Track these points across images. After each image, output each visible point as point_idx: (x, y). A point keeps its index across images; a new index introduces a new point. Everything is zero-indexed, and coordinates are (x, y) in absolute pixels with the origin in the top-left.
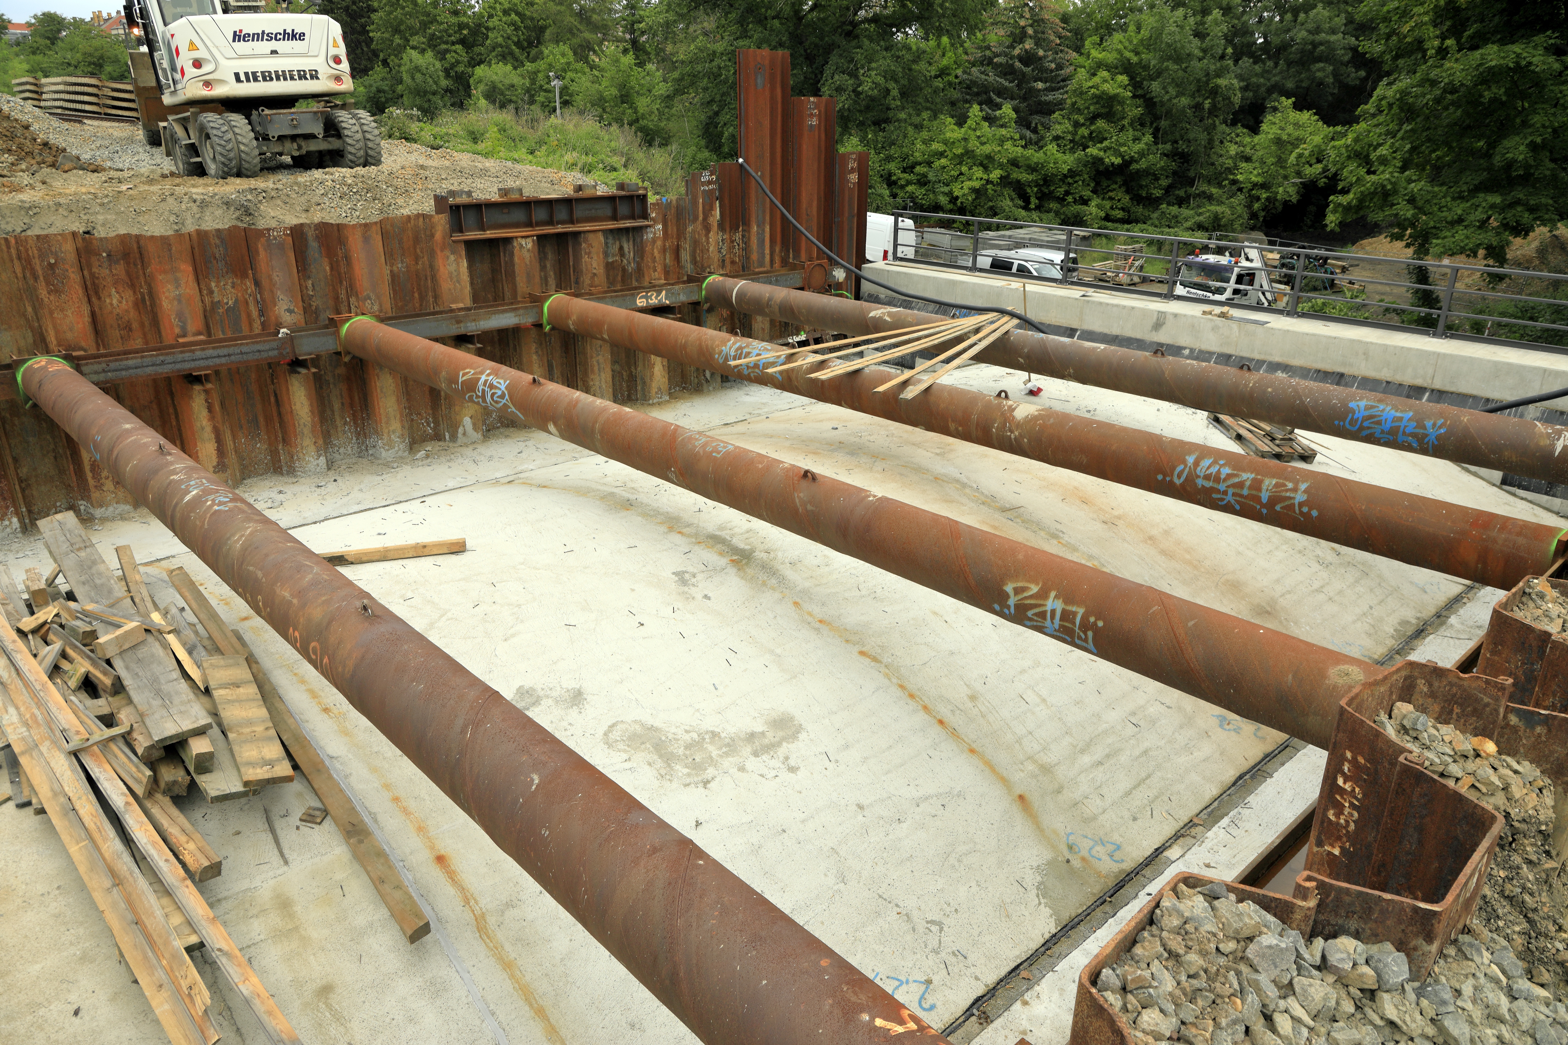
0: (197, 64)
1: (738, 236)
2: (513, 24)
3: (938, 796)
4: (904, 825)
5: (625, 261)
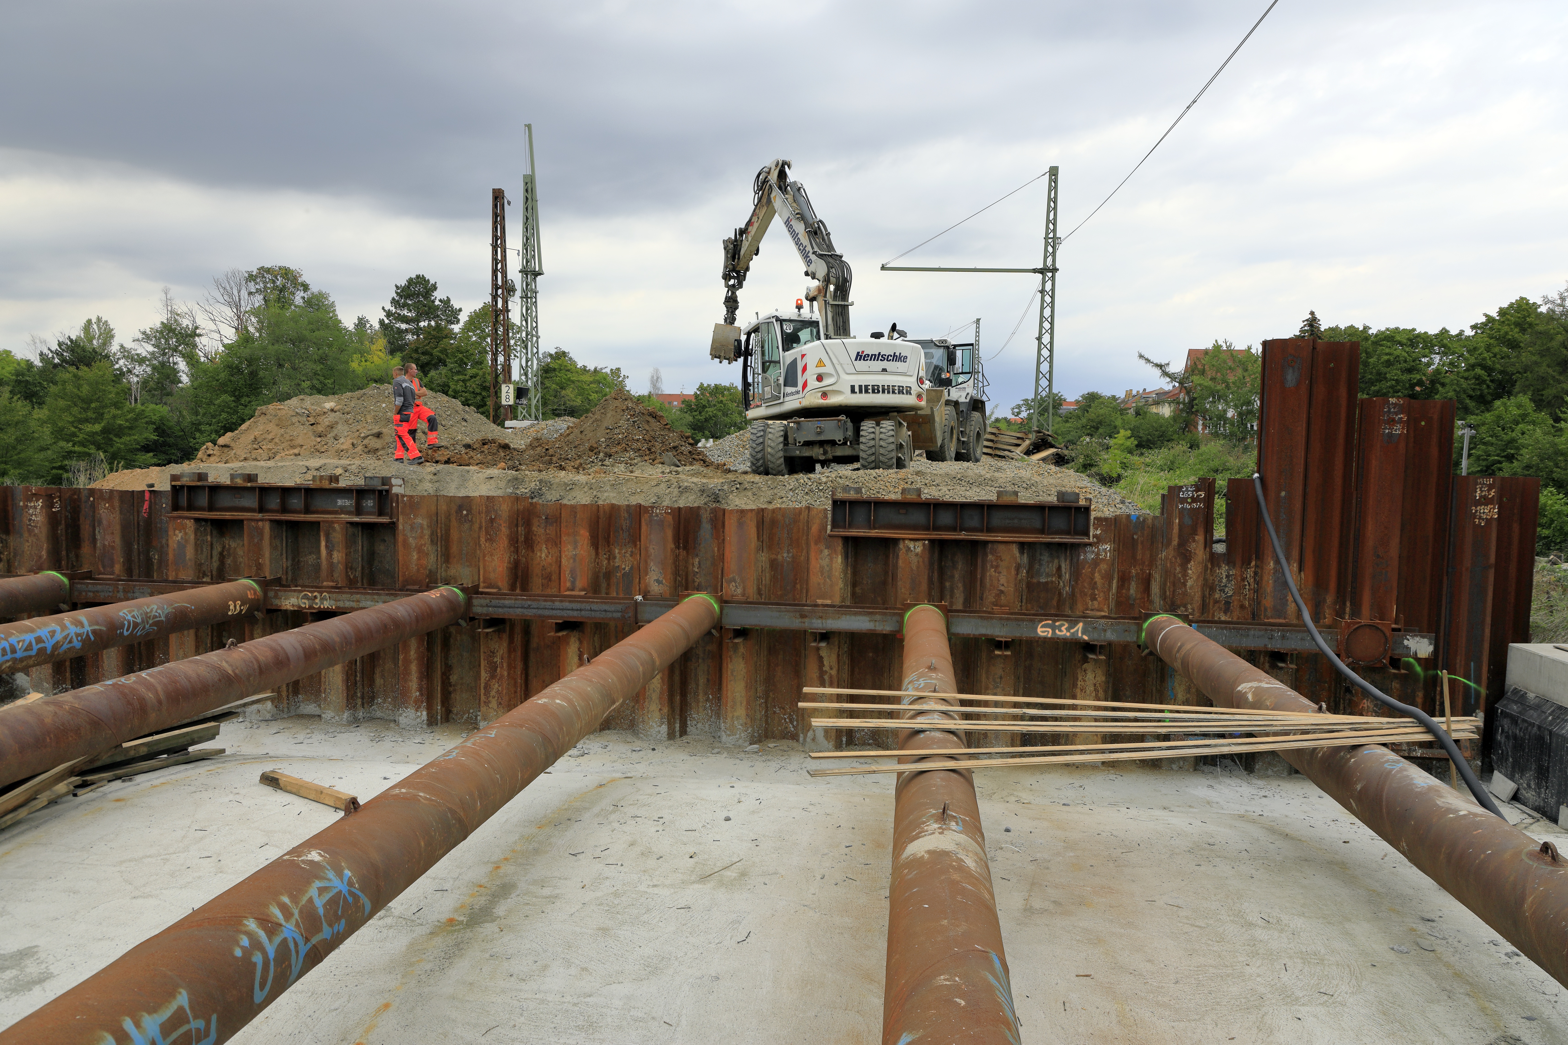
0: (820, 378)
1: (1250, 573)
2: (1478, 378)
5: (1062, 584)
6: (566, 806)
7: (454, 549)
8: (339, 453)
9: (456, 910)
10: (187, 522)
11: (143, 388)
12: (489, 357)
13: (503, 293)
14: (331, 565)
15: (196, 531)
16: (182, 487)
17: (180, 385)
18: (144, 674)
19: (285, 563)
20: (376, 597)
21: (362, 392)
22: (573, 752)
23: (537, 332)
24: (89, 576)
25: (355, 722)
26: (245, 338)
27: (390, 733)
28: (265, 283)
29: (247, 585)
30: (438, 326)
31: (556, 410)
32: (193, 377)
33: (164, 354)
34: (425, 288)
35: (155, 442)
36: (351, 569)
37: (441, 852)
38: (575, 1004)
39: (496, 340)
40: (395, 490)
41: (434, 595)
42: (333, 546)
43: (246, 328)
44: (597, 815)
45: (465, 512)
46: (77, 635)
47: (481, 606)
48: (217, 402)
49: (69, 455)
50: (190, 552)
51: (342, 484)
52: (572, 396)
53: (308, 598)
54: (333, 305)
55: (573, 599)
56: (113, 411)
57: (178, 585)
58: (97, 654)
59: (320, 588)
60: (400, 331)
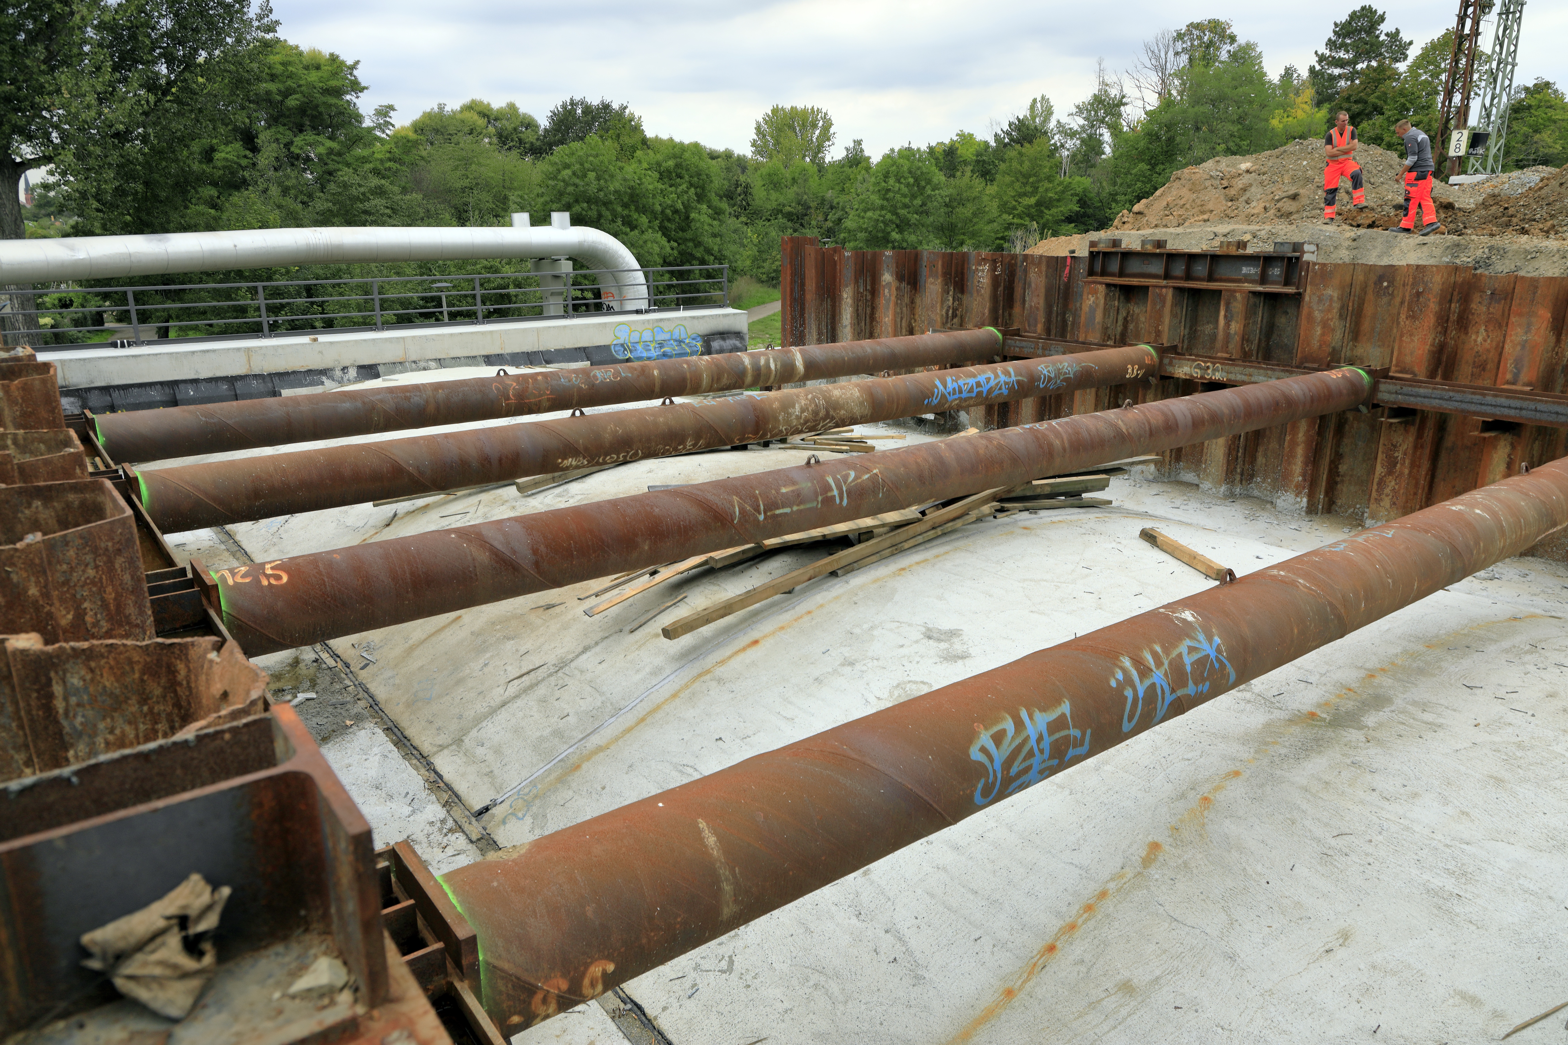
3: (909, 952)
4: (854, 920)
6: (1466, 631)
7: (1366, 325)
8: (1249, 218)
9: (1319, 705)
10: (1099, 286)
11: (1071, 162)
12: (1440, 98)
13: (1474, 12)
14: (1228, 336)
15: (1107, 295)
16: (1098, 253)
17: (1103, 156)
18: (1054, 422)
19: (1183, 331)
20: (1269, 372)
21: (1282, 149)
22: (1482, 573)
23: (1514, 59)
24: (1017, 333)
25: (1231, 497)
26: (1167, 103)
27: (1266, 514)
28: (1192, 40)
29: (1145, 350)
30: (1381, 64)
31: (1521, 161)
32: (1115, 147)
33: (1093, 126)
34: (1370, 21)
35: (1077, 213)
36: (1248, 341)
37: (1314, 644)
38: (1447, 846)
39: (1455, 73)
40: (1306, 257)
41: (1335, 375)
42: (1232, 317)
43: (1169, 91)
44: (1507, 651)
45: (1385, 284)
46: (1006, 383)
47: (1387, 393)
48: (1133, 172)
49: (1009, 226)
50: (1099, 316)
51: (1249, 251)
52: (1549, 140)
53: (1201, 369)
54: (1260, 55)
55: (1512, 394)
56: (1047, 185)
57: (1086, 346)
58: (1017, 402)
59: (1213, 359)
60: (1333, 78)
